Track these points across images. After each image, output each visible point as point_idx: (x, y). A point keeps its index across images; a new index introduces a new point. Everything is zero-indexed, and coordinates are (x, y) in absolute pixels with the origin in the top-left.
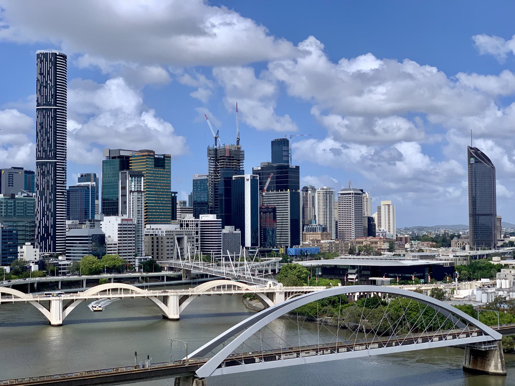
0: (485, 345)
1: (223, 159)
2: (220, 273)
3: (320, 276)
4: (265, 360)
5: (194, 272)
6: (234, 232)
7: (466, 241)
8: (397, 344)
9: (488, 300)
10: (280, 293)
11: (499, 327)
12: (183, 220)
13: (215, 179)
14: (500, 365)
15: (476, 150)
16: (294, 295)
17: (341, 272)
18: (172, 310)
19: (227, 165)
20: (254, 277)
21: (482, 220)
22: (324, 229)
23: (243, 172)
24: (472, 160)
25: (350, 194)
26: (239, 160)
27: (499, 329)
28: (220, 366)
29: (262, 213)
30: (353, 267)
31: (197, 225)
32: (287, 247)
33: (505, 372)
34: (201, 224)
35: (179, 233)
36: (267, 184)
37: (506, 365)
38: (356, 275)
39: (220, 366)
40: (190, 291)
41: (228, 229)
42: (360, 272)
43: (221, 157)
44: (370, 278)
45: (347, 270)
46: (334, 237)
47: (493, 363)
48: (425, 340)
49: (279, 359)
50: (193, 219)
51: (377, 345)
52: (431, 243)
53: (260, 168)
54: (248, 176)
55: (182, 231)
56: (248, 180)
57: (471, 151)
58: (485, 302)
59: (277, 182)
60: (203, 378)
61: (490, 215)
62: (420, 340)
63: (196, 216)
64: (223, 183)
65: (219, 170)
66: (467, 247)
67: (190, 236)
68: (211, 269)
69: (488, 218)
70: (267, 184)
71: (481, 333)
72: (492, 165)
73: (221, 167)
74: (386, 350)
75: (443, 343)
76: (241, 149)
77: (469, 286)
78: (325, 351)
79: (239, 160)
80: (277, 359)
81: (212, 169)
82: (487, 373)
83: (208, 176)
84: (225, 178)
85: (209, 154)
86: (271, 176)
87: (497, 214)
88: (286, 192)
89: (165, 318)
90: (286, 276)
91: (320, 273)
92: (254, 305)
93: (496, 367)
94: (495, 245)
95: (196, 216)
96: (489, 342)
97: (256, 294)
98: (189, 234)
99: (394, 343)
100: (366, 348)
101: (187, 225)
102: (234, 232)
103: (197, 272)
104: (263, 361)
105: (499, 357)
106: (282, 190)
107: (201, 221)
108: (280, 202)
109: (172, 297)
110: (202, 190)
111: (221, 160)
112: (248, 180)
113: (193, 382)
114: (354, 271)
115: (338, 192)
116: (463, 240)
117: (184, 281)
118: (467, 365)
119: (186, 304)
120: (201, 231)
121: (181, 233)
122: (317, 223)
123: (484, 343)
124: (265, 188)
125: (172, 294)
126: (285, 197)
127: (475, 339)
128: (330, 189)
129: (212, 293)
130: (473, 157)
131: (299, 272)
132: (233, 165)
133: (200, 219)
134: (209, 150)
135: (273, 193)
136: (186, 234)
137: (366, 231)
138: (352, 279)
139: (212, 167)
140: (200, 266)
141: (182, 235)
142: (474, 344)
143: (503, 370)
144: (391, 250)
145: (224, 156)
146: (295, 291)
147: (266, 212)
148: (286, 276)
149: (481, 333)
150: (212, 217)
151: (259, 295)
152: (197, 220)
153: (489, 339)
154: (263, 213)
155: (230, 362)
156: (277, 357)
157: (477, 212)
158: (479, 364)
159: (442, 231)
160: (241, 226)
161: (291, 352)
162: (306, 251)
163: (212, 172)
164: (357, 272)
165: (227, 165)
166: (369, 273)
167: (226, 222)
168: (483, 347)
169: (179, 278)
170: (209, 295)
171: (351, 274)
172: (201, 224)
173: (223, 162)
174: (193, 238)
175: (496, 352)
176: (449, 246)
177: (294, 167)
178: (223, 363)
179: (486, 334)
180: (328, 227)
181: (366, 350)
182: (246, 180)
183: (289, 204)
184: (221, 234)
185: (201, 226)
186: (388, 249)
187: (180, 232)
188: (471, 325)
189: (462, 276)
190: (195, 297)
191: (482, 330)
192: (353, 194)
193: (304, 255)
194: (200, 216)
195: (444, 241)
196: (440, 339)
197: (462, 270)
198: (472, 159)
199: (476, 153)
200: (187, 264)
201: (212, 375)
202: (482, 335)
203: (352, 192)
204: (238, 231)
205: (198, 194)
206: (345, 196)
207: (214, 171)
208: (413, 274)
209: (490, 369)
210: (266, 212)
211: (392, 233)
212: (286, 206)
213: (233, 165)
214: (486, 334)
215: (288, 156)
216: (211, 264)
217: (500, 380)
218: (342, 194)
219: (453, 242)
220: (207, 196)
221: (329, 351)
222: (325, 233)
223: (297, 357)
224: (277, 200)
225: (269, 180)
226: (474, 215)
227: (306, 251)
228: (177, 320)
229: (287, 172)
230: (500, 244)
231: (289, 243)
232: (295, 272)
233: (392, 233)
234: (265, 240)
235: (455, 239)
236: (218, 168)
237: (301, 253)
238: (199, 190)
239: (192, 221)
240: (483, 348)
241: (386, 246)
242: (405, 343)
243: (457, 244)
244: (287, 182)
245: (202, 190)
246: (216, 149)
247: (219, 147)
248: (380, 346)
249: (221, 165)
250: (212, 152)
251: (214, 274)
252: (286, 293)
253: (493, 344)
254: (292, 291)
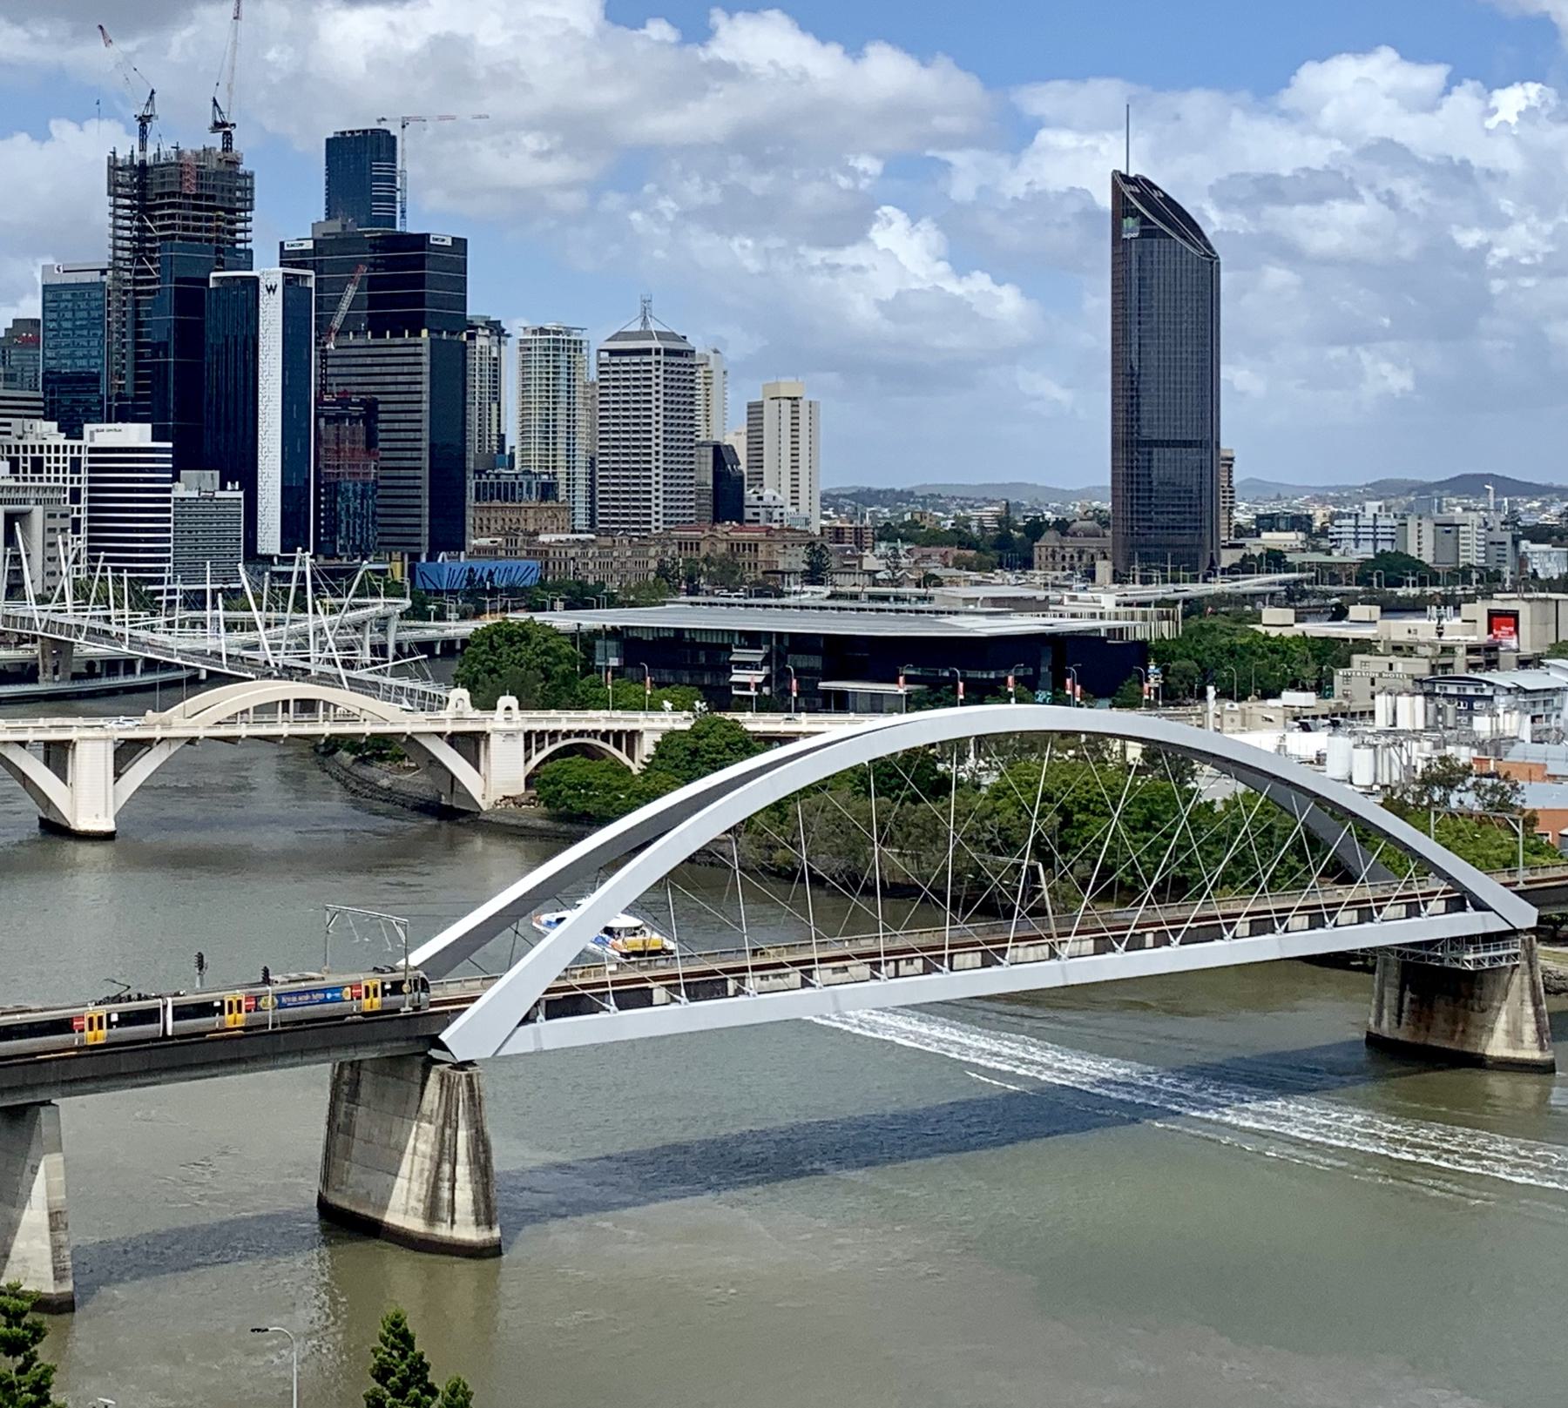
0: (1477, 950)
1: (171, 205)
2: (202, 653)
3: (617, 672)
4: (693, 997)
5: (90, 649)
6: (219, 494)
7: (1092, 545)
8: (1162, 940)
9: (1375, 775)
10: (510, 735)
11: (1523, 875)
12: (21, 443)
13: (136, 282)
14: (1529, 1030)
15: (1144, 187)
16: (561, 743)
17: (703, 659)
18: (91, 797)
19: (186, 228)
20: (353, 674)
21: (1165, 465)
22: (548, 491)
23: (247, 260)
24: (1131, 227)
25: (647, 352)
26: (233, 211)
27: (1521, 886)
28: (527, 1019)
29: (322, 422)
30: (753, 639)
31: (76, 465)
32: (415, 557)
33: (1548, 1056)
34: (91, 460)
35: (13, 495)
36: (344, 306)
37: (1556, 1027)
38: (765, 670)
39: (527, 1019)
40: (149, 725)
41: (193, 485)
42: (782, 659)
43: (162, 196)
44: (822, 685)
45: (727, 649)
46: (581, 521)
47: (1502, 1023)
48: (1261, 925)
49: (739, 992)
50: (61, 440)
51: (1089, 945)
52: (955, 551)
53: (309, 245)
54: (268, 271)
55: (25, 489)
56: (271, 289)
57: (1127, 189)
58: (1368, 783)
59: (374, 302)
60: (471, 1063)
61: (1198, 444)
62: (1242, 926)
63: (73, 431)
64: (169, 302)
65: (153, 250)
66: (1104, 569)
67: (53, 508)
68: (160, 637)
69: (1192, 455)
70: (344, 306)
71: (1460, 900)
72: (1209, 247)
73: (162, 238)
74: (1121, 964)
75: (1268, 947)
76: (242, 169)
77: (1238, 718)
78: (902, 963)
79: (233, 211)
80: (731, 992)
81: (127, 244)
82: (1479, 1062)
83: (103, 272)
84: (178, 281)
85: (114, 187)
86: (357, 276)
87: (1223, 446)
88: (413, 340)
89: (55, 829)
90: (491, 671)
91: (614, 662)
92: (385, 783)
93: (1515, 1036)
94: (1212, 563)
95: (73, 431)
96: (1489, 939)
97: (411, 739)
98: (50, 501)
99: (1149, 938)
100: (1053, 955)
101: (37, 465)
102: (219, 494)
103: (103, 650)
104: (684, 1000)
105: (1527, 997)
106: (397, 333)
107: (92, 450)
108: (388, 379)
109: (88, 745)
110: (82, 327)
111: (161, 207)
112: (271, 289)
113: (425, 1078)
114: (756, 656)
115: (597, 338)
116: (1081, 542)
117: (41, 687)
118: (1387, 1028)
119: (142, 769)
120: (91, 490)
121: (21, 495)
122: (517, 466)
123: (1471, 939)
124: (336, 324)
125: (89, 733)
126: (411, 359)
127: (1436, 924)
128: (568, 331)
129: (242, 731)
130: (1136, 213)
131: (544, 653)
132: (208, 230)
133: (86, 442)
134: (114, 167)
135: (361, 342)
136: (38, 502)
137: (707, 501)
138: (746, 686)
139: (127, 233)
140: (114, 629)
141: (25, 501)
142: (1430, 944)
143: (1542, 1049)
144: (814, 575)
145: (172, 194)
146: (564, 726)
147: (338, 419)
148: (491, 671)
149: (1460, 900)
150: (137, 434)
151: (422, 741)
152: (76, 443)
153: (1494, 925)
154: (328, 420)
155: (564, 1003)
156: (732, 985)
157: (1145, 431)
158: (1440, 1022)
159: (989, 513)
160: (243, 472)
161: (782, 965)
162: (491, 574)
163: (126, 254)
164: (767, 660)
165: (186, 228)
166: (816, 662)
167: (185, 459)
168: (1470, 957)
169: (27, 673)
170: (232, 740)
171: (743, 665)
172: (91, 460)
173: (172, 216)
174: (64, 516)
175: (1516, 979)
176: (1028, 564)
177: (449, 242)
178: (537, 1004)
179: (1480, 906)
180: (561, 476)
181: (1054, 962)
182: (263, 290)
183: (426, 387)
184: (168, 500)
185: (91, 470)
186: (804, 573)
187: (17, 489)
188: (1427, 867)
189: (1171, 680)
190: (176, 747)
191: (1466, 891)
192: (658, 352)
193: (483, 591)
194: (88, 428)
195: (1011, 543)
196: (1316, 922)
197: (1173, 657)
198: (1129, 222)
199: (1141, 197)
200: (59, 618)
201: (501, 1053)
202: (1464, 909)
203: (654, 344)
204: (234, 493)
205: (65, 341)
206: (626, 360)
207: (134, 250)
208: (1008, 668)
209: (1493, 1042)
210: (338, 419)
211: (804, 511)
212: (415, 397)
213: (208, 230)
214: (1480, 906)
215: (393, 199)
216: (162, 620)
217: (1529, 1087)
218: (613, 353)
219: (1042, 548)
220: (105, 357)
221: (919, 964)
222: (549, 504)
223: (805, 984)
224: (376, 370)
225: (351, 290)
226: (1131, 444)
227: (491, 574)
228: (108, 837)
229: (420, 262)
230: (1228, 558)
231: (425, 540)
232: (528, 654)
233: (804, 511)
234: (333, 530)
235: (1050, 539)
236: (151, 240)
237: (470, 581)
238: (66, 325)
239: (57, 449)
240: (1469, 958)
241: (797, 559)
242: (1191, 938)
243: (1058, 558)
244: (420, 300)
245: (82, 327)
246: (143, 163)
247: (157, 156)
248: (1103, 947)
249: (162, 228)
250: (124, 177)
251: (178, 660)
252: (528, 735)
253: (1506, 947)
254: (552, 727)
